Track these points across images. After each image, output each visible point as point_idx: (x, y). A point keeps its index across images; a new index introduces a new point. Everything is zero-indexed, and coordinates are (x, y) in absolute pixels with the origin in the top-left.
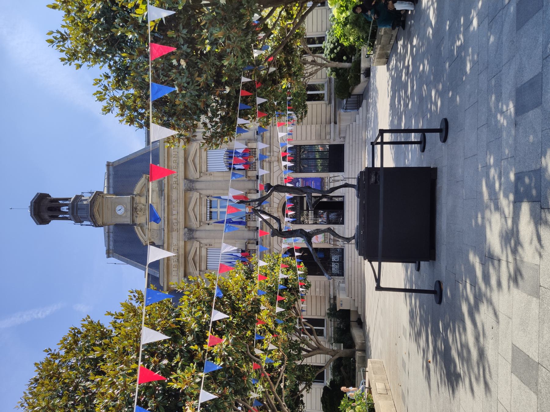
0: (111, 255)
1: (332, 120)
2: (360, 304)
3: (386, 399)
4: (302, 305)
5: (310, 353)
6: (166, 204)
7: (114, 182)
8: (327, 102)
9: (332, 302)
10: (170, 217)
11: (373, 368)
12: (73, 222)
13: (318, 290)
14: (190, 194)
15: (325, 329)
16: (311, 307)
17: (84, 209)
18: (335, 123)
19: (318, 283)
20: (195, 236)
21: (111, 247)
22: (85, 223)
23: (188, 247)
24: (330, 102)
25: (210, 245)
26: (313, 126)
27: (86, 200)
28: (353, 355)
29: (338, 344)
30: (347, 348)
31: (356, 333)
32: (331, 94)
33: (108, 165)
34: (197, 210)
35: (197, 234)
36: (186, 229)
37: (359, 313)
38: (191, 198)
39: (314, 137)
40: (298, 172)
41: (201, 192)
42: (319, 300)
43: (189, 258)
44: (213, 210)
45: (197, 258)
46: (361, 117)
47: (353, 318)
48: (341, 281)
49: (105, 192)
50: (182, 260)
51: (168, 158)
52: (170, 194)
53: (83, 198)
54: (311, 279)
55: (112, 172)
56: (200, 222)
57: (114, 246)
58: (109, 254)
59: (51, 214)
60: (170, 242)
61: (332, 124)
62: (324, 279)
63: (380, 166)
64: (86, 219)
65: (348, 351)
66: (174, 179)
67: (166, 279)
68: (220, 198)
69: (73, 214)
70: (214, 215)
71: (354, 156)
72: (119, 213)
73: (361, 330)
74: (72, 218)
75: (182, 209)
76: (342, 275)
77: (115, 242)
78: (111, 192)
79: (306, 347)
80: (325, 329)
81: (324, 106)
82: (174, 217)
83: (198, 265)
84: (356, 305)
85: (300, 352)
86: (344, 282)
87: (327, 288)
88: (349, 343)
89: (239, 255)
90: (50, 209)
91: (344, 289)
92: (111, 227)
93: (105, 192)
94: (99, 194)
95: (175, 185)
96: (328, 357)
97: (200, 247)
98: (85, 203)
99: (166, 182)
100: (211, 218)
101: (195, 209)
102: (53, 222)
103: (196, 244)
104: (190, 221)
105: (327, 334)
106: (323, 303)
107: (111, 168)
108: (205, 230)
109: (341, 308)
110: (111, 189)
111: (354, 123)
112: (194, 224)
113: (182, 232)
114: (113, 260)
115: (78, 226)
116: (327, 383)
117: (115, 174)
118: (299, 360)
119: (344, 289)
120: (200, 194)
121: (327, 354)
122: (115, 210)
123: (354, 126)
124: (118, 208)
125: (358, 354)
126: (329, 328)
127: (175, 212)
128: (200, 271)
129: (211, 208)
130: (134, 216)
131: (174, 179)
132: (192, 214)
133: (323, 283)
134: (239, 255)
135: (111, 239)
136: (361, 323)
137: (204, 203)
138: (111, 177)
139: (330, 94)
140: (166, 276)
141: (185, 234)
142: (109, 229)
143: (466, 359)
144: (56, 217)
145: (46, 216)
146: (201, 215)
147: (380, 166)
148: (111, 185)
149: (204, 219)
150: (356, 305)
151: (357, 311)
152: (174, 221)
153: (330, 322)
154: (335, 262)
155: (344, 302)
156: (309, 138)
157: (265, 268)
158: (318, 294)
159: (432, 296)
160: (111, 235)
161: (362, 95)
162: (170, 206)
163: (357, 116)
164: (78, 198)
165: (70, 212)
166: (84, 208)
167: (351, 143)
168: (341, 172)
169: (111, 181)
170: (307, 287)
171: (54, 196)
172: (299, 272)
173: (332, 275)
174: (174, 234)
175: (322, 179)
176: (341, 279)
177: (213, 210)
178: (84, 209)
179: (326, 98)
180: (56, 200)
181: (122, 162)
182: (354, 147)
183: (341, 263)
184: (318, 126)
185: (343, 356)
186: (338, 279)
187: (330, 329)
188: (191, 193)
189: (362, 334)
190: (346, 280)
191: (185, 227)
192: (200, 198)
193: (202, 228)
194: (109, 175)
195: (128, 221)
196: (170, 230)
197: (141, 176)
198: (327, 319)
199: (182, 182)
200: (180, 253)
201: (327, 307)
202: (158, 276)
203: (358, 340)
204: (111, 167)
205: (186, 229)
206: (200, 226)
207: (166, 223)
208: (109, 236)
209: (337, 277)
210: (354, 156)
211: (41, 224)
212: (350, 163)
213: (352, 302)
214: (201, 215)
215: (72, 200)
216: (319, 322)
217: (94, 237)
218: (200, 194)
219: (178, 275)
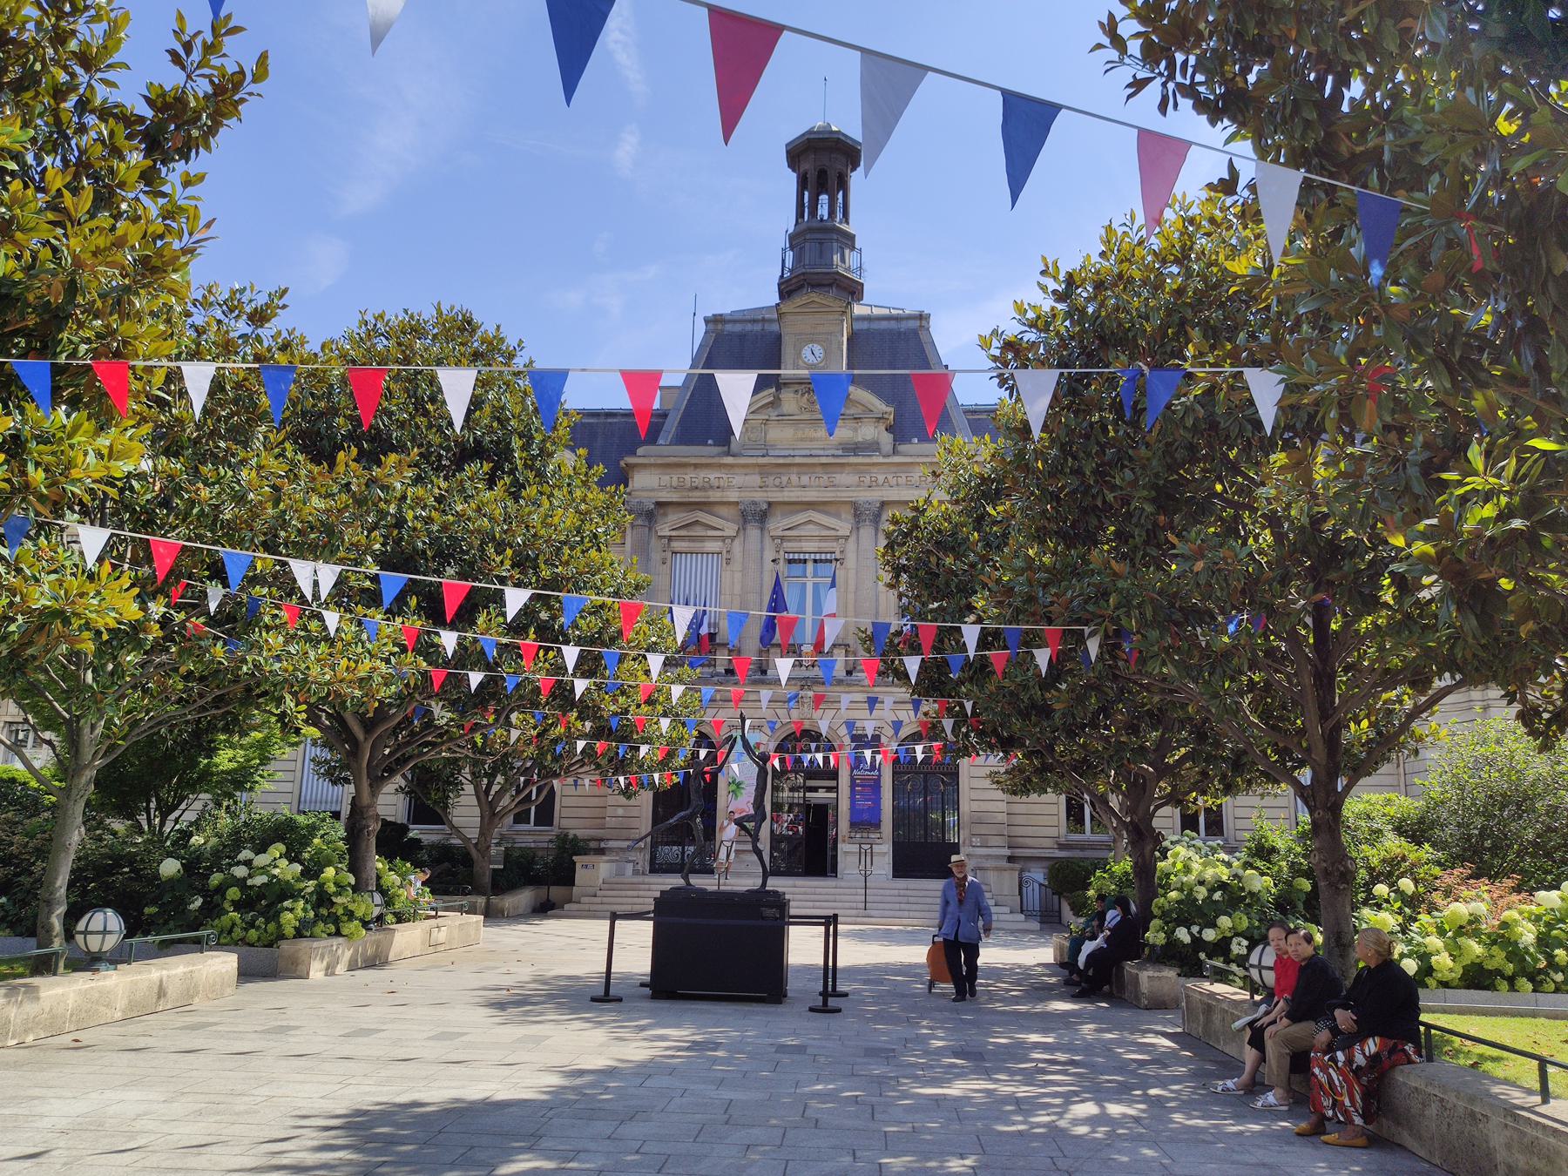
0: (711, 326)
1: (1019, 852)
3: (423, 943)
4: (587, 782)
5: (482, 794)
6: (824, 460)
7: (881, 333)
8: (1062, 840)
9: (593, 845)
10: (795, 470)
11: (468, 924)
12: (791, 230)
13: (620, 812)
14: (847, 515)
15: (531, 826)
16: (579, 799)
17: (821, 256)
18: (1011, 859)
19: (635, 812)
20: (749, 527)
21: (729, 327)
22: (790, 255)
23: (723, 511)
24: (1062, 847)
25: (728, 560)
26: (1003, 806)
27: (843, 260)
28: (478, 891)
29: (501, 858)
30: (493, 879)
31: (523, 898)
32: (1082, 848)
33: (922, 317)
34: (811, 530)
35: (753, 532)
36: (765, 506)
37: (567, 907)
38: (837, 516)
39: (975, 806)
41: (852, 540)
42: (597, 813)
43: (700, 514)
44: (810, 566)
45: (698, 531)
47: (556, 892)
48: (639, 867)
49: (858, 310)
50: (696, 496)
52: (848, 469)
53: (847, 252)
54: (646, 799)
55: (904, 326)
56: (782, 538)
57: (731, 334)
58: (714, 321)
59: (812, 177)
60: (737, 470)
61: (1007, 852)
62: (645, 825)
64: (798, 259)
65: (487, 880)
66: (881, 478)
67: (652, 460)
69: (810, 230)
70: (797, 568)
72: (806, 352)
74: (802, 227)
75: (811, 495)
76: (653, 870)
77: (742, 337)
78: (857, 326)
79: (495, 788)
80: (531, 826)
81: (1053, 832)
82: (794, 478)
83: (683, 533)
84: (584, 899)
85: (486, 774)
86: (636, 872)
87: (625, 833)
88: (503, 883)
89: (704, 631)
90: (822, 174)
91: (620, 873)
92: (775, 327)
93: (858, 310)
94: (853, 291)
95: (867, 480)
96: (473, 834)
97: (723, 538)
98: (836, 258)
99: (874, 460)
100: (790, 561)
101: (811, 526)
102: (791, 179)
103: (730, 529)
104: (785, 515)
105: (518, 833)
106: (588, 823)
107: (913, 324)
108: (762, 550)
109: (578, 866)
110: (864, 325)
112: (777, 525)
113: (760, 497)
114: (701, 328)
115: (782, 241)
116: (415, 832)
117: (899, 333)
118: (473, 774)
119: (620, 873)
120: (847, 538)
121: (481, 834)
122: (812, 341)
124: (818, 349)
125: (481, 901)
126: (531, 836)
127: (805, 479)
128: (670, 538)
129: (815, 561)
130: (797, 387)
131: (881, 478)
132: (800, 518)
133: (634, 823)
134: (704, 631)
135: (749, 327)
136: (544, 909)
137: (826, 546)
138: (893, 325)
139: (1082, 847)
140: (660, 461)
141: (754, 503)
142: (771, 321)
143: (526, 1013)
144: (803, 184)
145: (806, 166)
146: (799, 538)
148: (875, 326)
149: (788, 545)
150: (584, 899)
151: (570, 901)
152: (785, 479)
153: (547, 838)
155: (593, 872)
156: (974, 795)
157: (669, 698)
158: (610, 811)
159: (601, 992)
160: (758, 327)
161: (1060, 922)
162: (818, 469)
163: (1007, 910)
164: (849, 240)
165: (815, 224)
166: (824, 255)
169: (884, 325)
170: (627, 793)
171: (856, 179)
172: (656, 776)
173: (654, 845)
174: (755, 480)
175: (877, 825)
177: (810, 566)
178: (821, 256)
180: (843, 184)
181: (927, 348)
184: (1002, 818)
185: (476, 869)
186: (643, 859)
187: (530, 838)
188: (850, 517)
189: (521, 911)
190: (640, 879)
191: (770, 504)
192: (837, 538)
193: (767, 541)
194: (897, 318)
196: (763, 470)
197: (888, 403)
198: (555, 830)
199: (876, 496)
200: (710, 493)
201: (581, 833)
202: (661, 441)
203: (509, 901)
204: (918, 323)
205: (765, 506)
206: (773, 538)
207: (781, 461)
208: (754, 321)
209: (648, 857)
211: (788, 152)
213: (591, 891)
214: (799, 538)
215: (844, 227)
216: (546, 815)
217: (753, 287)
218: (847, 538)
219: (662, 488)
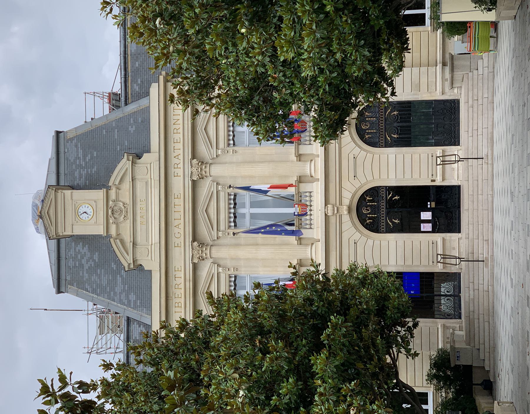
2: (487, 355)
40: (382, 147)
46: (486, 65)
47: (477, 378)
51: (493, 175)
63: (422, 218)
68: (247, 189)
71: (475, 122)
73: (490, 397)
81: (424, 36)
109: (458, 363)
111: (475, 72)
123: (475, 77)
147: (422, 218)
150: (482, 357)
154: (446, 296)
167: (470, 102)
168: (455, 145)
176: (458, 323)
179: (428, 21)
181: (80, 132)
182: (475, 109)
183: (456, 296)
195: (100, 231)
210: (475, 122)
212: (470, 134)
